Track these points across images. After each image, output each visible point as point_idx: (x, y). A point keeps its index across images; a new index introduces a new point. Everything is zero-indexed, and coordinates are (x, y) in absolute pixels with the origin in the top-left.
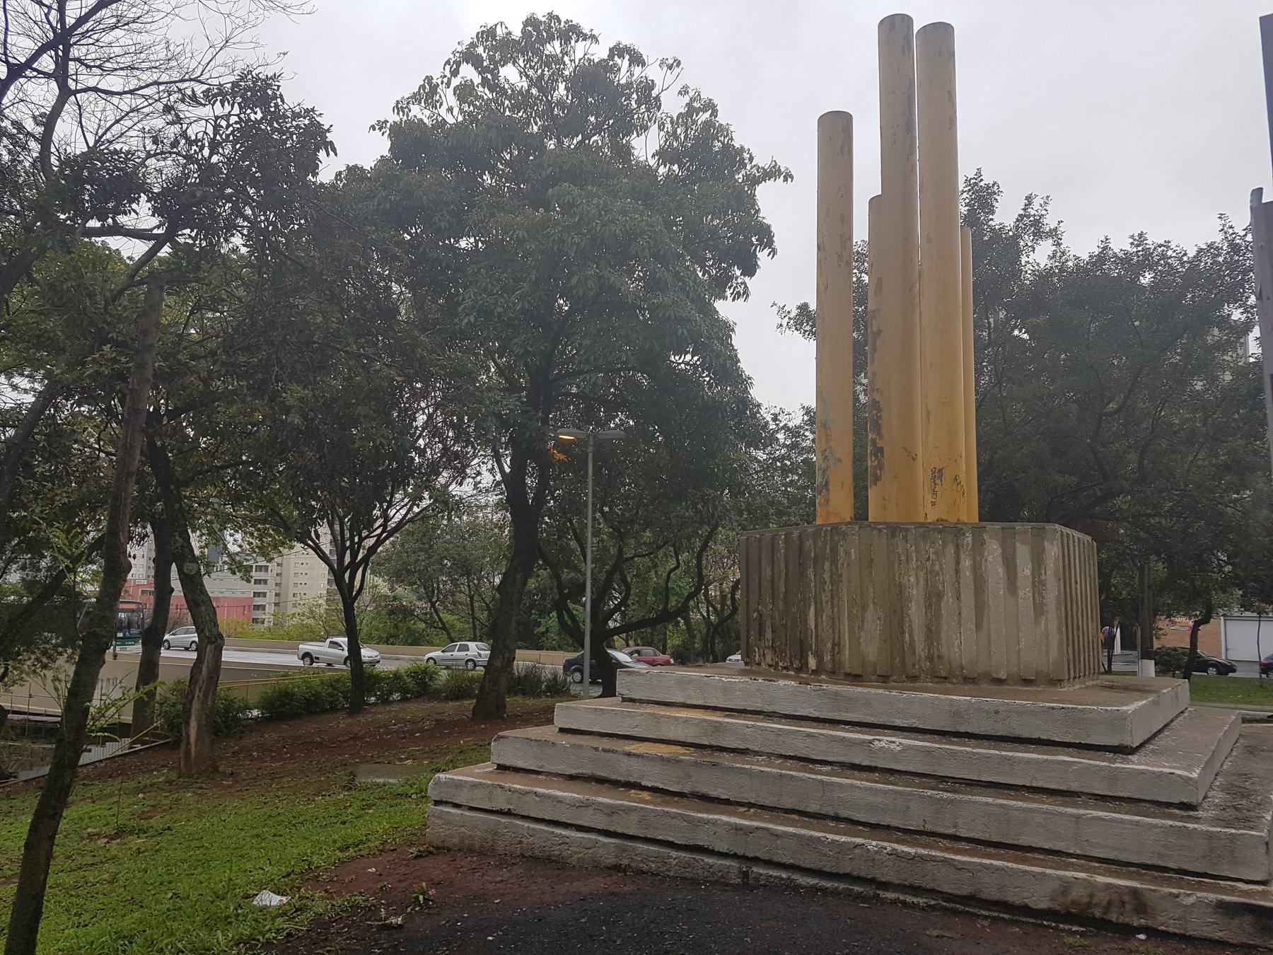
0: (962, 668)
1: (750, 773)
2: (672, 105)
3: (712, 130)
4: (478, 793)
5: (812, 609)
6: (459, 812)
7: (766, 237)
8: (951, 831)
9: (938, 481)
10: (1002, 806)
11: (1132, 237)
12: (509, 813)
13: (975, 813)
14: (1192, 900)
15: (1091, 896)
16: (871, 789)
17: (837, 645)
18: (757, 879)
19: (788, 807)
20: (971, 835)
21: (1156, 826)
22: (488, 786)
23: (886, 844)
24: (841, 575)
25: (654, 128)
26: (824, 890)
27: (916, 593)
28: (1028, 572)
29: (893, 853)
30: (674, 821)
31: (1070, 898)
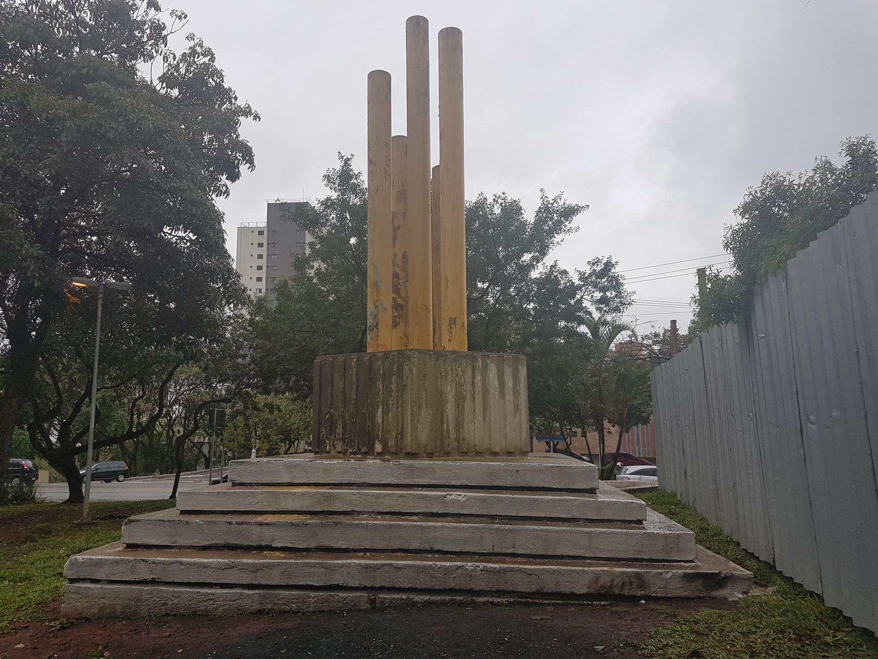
0: (475, 446)
1: (366, 527)
2: (177, 45)
3: (209, 70)
4: (121, 568)
5: (380, 410)
6: (99, 586)
7: (248, 156)
8: (511, 551)
9: (453, 326)
10: (543, 530)
11: (495, 195)
12: (153, 582)
13: (527, 537)
14: (669, 575)
15: (612, 581)
16: (456, 527)
17: (401, 434)
18: (382, 602)
19: (395, 547)
20: (524, 552)
21: (636, 534)
22: (131, 561)
23: (478, 564)
24: (406, 385)
25: (159, 59)
26: (434, 603)
27: (450, 397)
28: (511, 384)
29: (485, 570)
30: (313, 570)
31: (600, 584)
